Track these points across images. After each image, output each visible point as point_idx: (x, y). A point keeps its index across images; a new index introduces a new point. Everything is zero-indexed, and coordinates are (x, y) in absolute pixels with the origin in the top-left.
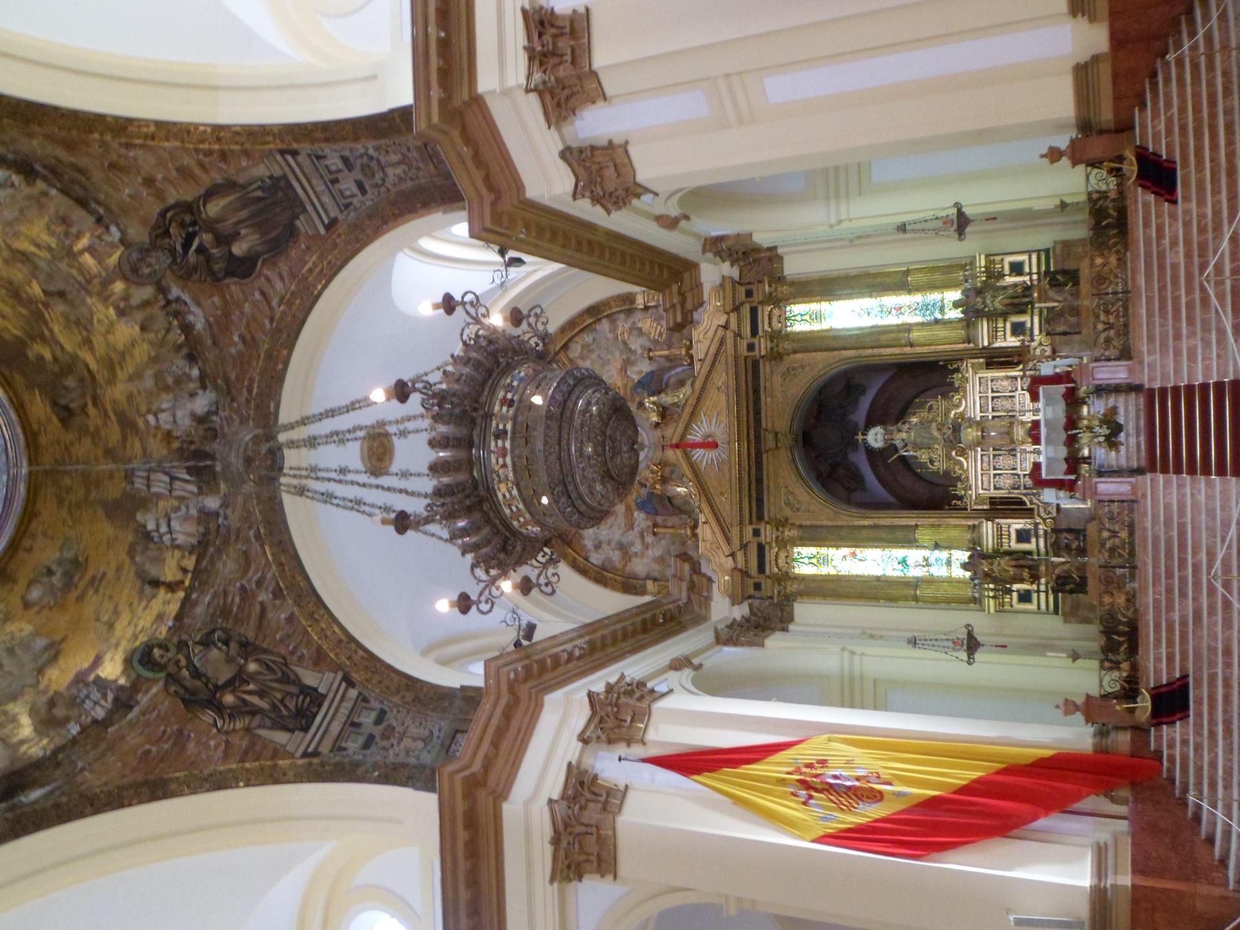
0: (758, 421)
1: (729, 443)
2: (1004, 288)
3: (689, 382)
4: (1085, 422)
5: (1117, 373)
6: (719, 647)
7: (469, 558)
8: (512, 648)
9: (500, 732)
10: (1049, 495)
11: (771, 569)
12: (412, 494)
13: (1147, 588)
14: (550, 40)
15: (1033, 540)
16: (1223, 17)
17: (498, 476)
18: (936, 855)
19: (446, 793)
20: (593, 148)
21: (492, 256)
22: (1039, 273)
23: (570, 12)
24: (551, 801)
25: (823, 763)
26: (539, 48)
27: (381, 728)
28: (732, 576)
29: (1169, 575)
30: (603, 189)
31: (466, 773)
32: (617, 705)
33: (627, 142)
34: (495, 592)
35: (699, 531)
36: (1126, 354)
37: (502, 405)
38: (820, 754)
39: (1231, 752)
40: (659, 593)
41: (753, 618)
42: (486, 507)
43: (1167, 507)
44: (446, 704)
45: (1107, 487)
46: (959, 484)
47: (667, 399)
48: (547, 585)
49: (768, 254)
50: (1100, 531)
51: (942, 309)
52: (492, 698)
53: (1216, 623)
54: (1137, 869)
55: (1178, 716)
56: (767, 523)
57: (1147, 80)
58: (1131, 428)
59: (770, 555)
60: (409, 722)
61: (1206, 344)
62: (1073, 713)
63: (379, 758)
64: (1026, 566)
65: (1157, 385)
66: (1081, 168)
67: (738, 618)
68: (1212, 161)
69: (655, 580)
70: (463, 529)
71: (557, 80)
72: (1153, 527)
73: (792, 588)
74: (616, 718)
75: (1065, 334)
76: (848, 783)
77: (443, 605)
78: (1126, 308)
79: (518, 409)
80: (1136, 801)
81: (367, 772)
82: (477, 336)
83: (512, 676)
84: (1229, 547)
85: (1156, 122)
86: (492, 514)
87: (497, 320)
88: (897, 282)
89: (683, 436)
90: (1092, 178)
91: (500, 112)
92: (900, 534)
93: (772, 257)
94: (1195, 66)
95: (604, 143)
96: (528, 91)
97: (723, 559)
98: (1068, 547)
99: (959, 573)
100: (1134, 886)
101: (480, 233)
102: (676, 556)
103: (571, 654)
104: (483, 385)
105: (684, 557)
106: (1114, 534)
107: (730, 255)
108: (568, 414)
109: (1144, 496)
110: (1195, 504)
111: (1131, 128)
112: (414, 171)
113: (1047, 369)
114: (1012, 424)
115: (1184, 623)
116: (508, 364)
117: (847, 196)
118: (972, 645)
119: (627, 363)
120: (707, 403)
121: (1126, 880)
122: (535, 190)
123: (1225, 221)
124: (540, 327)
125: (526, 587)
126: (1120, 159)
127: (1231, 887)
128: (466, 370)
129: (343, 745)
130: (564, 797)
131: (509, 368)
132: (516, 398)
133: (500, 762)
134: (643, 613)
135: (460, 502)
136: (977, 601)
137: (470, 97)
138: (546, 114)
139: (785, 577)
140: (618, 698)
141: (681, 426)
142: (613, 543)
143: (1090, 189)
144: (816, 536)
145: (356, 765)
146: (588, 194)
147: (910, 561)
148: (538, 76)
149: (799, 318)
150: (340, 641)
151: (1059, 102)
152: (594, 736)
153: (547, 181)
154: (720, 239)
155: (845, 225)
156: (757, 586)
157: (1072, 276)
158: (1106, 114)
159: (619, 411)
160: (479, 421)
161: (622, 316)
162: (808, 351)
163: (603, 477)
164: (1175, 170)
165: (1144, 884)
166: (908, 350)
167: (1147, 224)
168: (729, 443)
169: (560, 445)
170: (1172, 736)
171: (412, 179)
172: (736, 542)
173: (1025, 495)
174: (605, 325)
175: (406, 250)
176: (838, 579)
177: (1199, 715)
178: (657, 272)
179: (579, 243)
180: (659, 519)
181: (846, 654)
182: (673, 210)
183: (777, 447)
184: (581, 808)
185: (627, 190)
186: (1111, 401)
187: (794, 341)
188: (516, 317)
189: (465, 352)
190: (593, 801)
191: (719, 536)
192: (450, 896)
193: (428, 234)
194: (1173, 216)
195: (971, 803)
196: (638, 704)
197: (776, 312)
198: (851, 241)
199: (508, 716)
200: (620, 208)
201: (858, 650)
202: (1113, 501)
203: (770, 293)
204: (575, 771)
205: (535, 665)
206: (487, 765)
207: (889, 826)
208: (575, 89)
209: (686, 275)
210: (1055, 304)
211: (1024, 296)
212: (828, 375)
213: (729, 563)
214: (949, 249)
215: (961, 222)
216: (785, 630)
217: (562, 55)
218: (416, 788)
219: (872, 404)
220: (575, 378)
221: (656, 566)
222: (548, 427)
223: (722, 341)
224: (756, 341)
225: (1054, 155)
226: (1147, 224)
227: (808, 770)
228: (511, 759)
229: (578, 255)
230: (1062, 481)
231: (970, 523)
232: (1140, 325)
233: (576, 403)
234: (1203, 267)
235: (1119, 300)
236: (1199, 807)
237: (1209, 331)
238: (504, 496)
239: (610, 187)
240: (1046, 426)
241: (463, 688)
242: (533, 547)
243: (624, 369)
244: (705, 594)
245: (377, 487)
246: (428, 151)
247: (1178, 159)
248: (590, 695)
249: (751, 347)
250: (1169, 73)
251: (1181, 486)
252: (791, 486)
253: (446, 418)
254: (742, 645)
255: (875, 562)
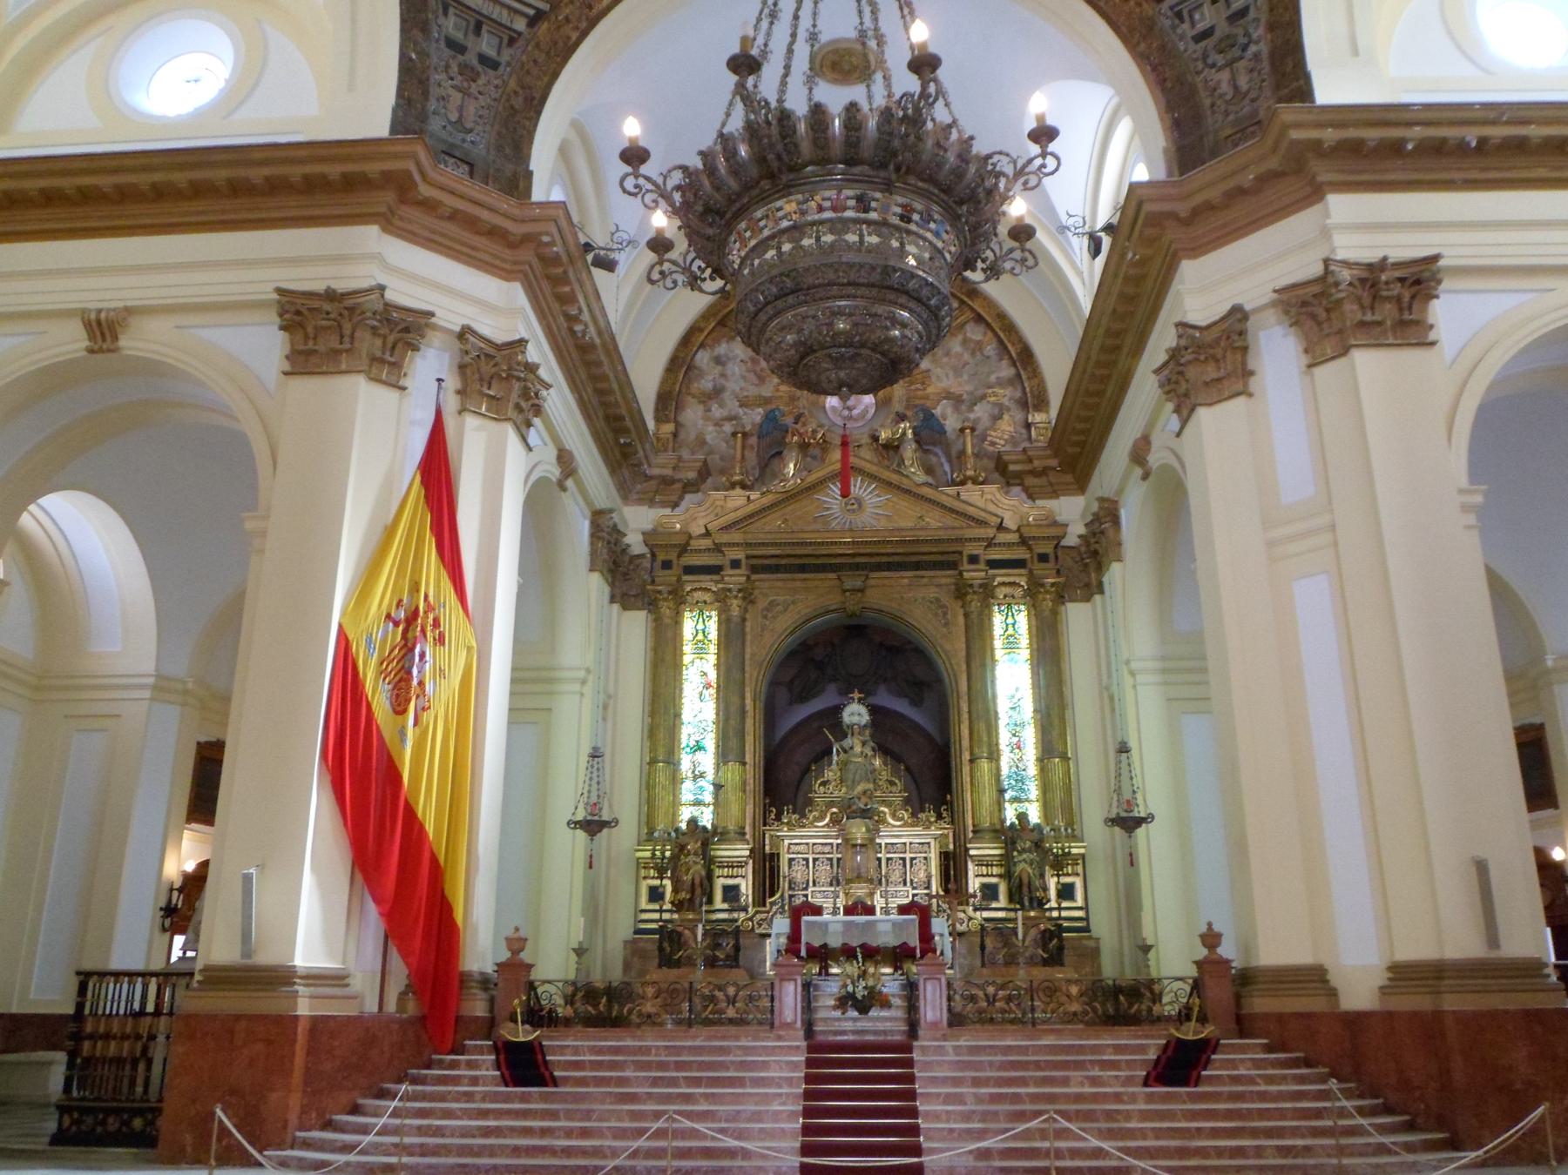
0: (879, 567)
1: (851, 530)
2: (1042, 876)
3: (930, 480)
4: (871, 970)
5: (933, 1007)
6: (588, 513)
7: (696, 163)
8: (583, 240)
9: (471, 223)
10: (781, 925)
11: (690, 583)
12: (783, 83)
13: (664, 1038)
14: (1395, 292)
15: (726, 906)
16: (1382, 1149)
17: (807, 201)
18: (328, 779)
19: (392, 149)
20: (1245, 349)
21: (1105, 213)
22: (1060, 918)
23: (1430, 321)
24: (382, 288)
25: (441, 640)
26: (1383, 278)
27: (475, 62)
28: (680, 532)
29: (680, 1066)
30: (1190, 362)
31: (417, 177)
32: (509, 377)
33: (1250, 395)
34: (649, 198)
35: (738, 491)
36: (956, 1020)
37: (903, 206)
38: (452, 635)
39: (463, 1136)
40: (658, 439)
41: (627, 559)
42: (766, 184)
43: (765, 1066)
44: (508, 151)
45: (790, 995)
46: (796, 816)
47: (909, 451)
48: (662, 273)
49: (1094, 582)
50: (735, 984)
51: (1016, 800)
52: (516, 212)
53: (620, 1120)
54: (317, 1023)
55: (507, 1073)
56: (748, 578)
57: (1301, 1055)
58: (863, 1024)
59: (706, 581)
60: (482, 100)
61: (967, 1117)
62: (510, 949)
63: (434, 59)
64: (695, 894)
65: (916, 1056)
66: (1192, 972)
67: (627, 540)
68: (1198, 1129)
69: (675, 435)
70: (735, 152)
71: (1340, 301)
72: (739, 1047)
73: (666, 609)
74: (492, 376)
75: (983, 947)
76: (415, 671)
77: (632, 128)
78: (1012, 1022)
79: (897, 228)
80: (401, 1022)
81: (416, 43)
82: (998, 175)
83: (546, 239)
84: (713, 1138)
85: (1249, 1064)
86: (755, 192)
87: (1017, 208)
88: (1053, 744)
89: (860, 471)
90: (1180, 984)
91: (1299, 225)
92: (734, 743)
93: (1090, 588)
94: (1318, 1114)
95: (1251, 365)
96: (1327, 262)
97: (702, 522)
98: (717, 946)
99: (685, 814)
100: (296, 1017)
101: (1136, 197)
102: (705, 461)
103: (575, 319)
104: (931, 180)
105: (705, 472)
106: (732, 1001)
107: (1094, 534)
108: (891, 296)
109: (779, 1038)
110: (767, 1098)
111: (1242, 1034)
112: (1223, 108)
113: (939, 925)
114: (871, 881)
115: (621, 1082)
116: (959, 217)
117: (1165, 683)
118: (593, 826)
119: (957, 400)
120: (903, 503)
121: (304, 1008)
122: (1189, 270)
123: (1121, 1144)
124: (1008, 265)
125: (659, 245)
126: (1203, 1020)
127: (299, 1134)
128: (951, 157)
129: (451, 10)
130: (389, 306)
131: (953, 218)
132: (913, 227)
133: (428, 220)
134: (632, 418)
135: (772, 146)
136: (650, 837)
137: (1323, 183)
138: (1294, 286)
139: (679, 600)
140: (519, 379)
141: (869, 467)
142: (722, 381)
143: (1166, 982)
144: (732, 640)
145: (425, 29)
146: (1183, 342)
147: (699, 755)
148: (1346, 275)
149: (1010, 620)
150: (590, 7)
151: (1278, 947)
152: (469, 347)
153: (1202, 290)
154: (1116, 521)
155: (1128, 680)
156: (667, 565)
157: (1055, 959)
158: (1260, 1004)
159: (887, 368)
160: (883, 174)
161: (1018, 394)
162: (967, 628)
163: (804, 343)
164: (1186, 1084)
165: (300, 1030)
166: (966, 756)
167: (1119, 1049)
168: (851, 530)
169: (849, 284)
170: (484, 1065)
171: (1213, 105)
172: (724, 538)
173: (782, 896)
174: (1006, 371)
175: (1116, 100)
176: (677, 666)
177: (507, 1098)
178: (1075, 438)
179: (1117, 334)
180: (753, 440)
181: (582, 674)
182: (1155, 458)
183: (845, 591)
184: (373, 328)
185: (1186, 395)
186: (897, 1001)
187: (980, 614)
188: (1022, 233)
189: (977, 156)
190: (384, 344)
191: (733, 517)
192: (257, 156)
193: (1138, 130)
194: (1129, 1081)
195: (394, 823)
196: (511, 405)
197: (1018, 592)
198: (1107, 688)
199: (494, 233)
200: (1161, 386)
201: (588, 689)
202: (772, 1000)
203: (1043, 585)
204: (423, 321)
205: (560, 270)
206: (429, 205)
207: (363, 719)
208: (1325, 326)
209: (1069, 478)
210: (1020, 936)
211: (1031, 900)
212: (935, 656)
213: (697, 529)
214: (1093, 810)
215: (1128, 822)
216: (613, 600)
217: (1372, 308)
218: (394, 111)
219: (902, 715)
220: (939, 308)
221: (692, 436)
222: (873, 268)
223: (981, 523)
224: (982, 566)
225: (1211, 939)
226: (1119, 1049)
227: (430, 620)
228: (437, 238)
229: (1101, 331)
230: (799, 941)
231: (748, 829)
232: (993, 1038)
233: (903, 307)
234: (1064, 1114)
235: (1024, 1014)
236: (392, 1096)
237: (983, 1121)
238: (780, 209)
239: (1192, 372)
240: (868, 922)
241: (529, 175)
242: (711, 253)
243: (948, 395)
244: (658, 498)
245: (794, 35)
246: (1251, 126)
247: (1199, 1089)
248: (521, 343)
249: (973, 559)
250: (1311, 1083)
251: (790, 1081)
252: (795, 608)
253: (886, 128)
254: (592, 544)
255: (699, 711)
